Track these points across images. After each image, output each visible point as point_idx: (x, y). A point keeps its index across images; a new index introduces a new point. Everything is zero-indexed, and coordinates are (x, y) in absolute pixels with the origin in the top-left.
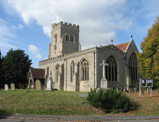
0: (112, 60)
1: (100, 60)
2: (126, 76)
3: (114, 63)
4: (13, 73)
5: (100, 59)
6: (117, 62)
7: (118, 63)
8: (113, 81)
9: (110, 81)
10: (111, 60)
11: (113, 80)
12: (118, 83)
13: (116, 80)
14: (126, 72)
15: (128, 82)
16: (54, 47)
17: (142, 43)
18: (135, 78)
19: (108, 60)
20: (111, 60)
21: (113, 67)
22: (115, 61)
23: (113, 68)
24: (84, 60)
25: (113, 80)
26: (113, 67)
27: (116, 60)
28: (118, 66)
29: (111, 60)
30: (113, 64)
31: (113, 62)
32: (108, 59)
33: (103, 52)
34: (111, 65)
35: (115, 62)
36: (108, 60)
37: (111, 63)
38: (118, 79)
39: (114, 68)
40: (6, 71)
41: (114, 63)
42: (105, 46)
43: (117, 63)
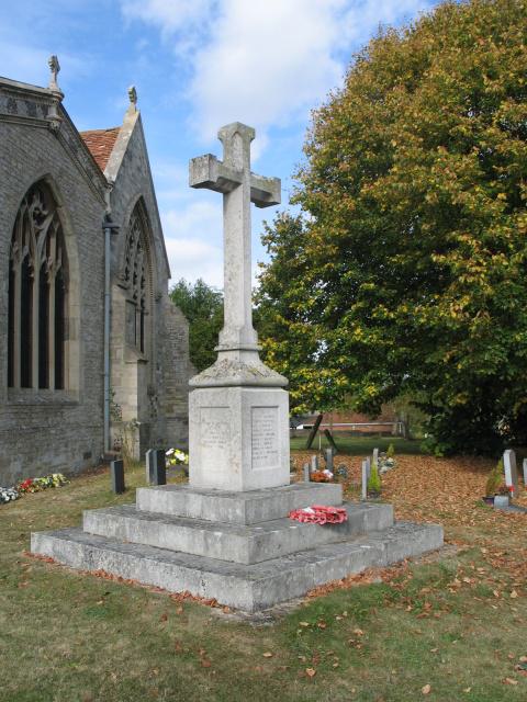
0: (45, 217)
2: (120, 352)
3: (53, 241)
6: (70, 242)
7: (80, 251)
9: (28, 390)
10: (40, 219)
11: (43, 384)
12: (74, 404)
13: (59, 385)
14: (115, 323)
15: (133, 400)
16: (192, 361)
18: (31, 280)
22: (60, 228)
24: (194, 161)
25: (43, 384)
27: (67, 228)
28: (75, 275)
32: (23, 202)
35: (61, 244)
37: (37, 235)
38: (73, 378)
41: (53, 241)
42: (13, 84)
43: (72, 253)
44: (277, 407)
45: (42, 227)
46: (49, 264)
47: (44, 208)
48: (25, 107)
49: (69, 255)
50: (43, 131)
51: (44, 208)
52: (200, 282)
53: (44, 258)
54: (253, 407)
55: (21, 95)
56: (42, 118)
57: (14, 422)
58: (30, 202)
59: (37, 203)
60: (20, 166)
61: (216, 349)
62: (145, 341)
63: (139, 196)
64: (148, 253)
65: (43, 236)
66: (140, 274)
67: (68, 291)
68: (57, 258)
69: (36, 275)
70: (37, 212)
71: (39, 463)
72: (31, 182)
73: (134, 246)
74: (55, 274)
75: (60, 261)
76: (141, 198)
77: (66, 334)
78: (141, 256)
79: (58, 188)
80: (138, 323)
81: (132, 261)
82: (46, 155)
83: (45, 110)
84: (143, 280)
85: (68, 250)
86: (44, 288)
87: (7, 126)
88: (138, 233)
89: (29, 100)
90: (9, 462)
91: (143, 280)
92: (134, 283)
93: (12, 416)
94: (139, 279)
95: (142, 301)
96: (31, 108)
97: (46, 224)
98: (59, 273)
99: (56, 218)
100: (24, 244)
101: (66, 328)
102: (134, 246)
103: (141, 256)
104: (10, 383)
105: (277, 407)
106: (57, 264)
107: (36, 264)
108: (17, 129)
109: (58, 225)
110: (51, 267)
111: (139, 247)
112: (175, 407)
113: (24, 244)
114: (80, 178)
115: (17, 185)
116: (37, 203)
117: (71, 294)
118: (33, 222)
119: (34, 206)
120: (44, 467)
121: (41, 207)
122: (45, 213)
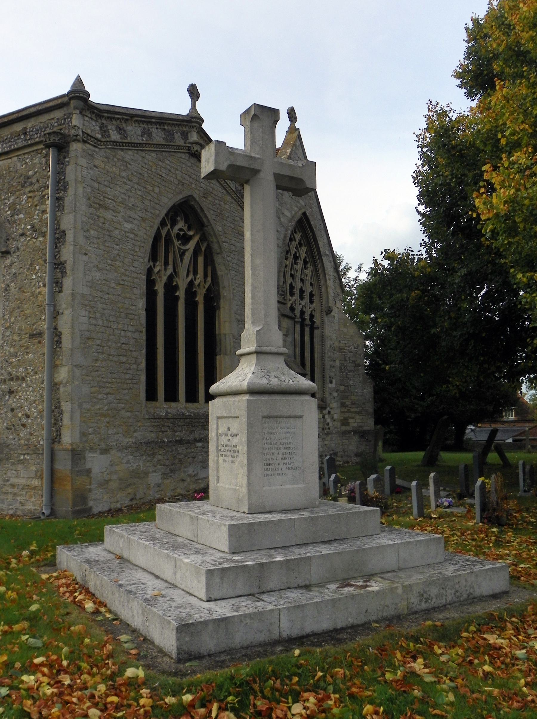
0: (190, 238)
1: (108, 215)
3: (201, 260)
4: (443, 658)
5: (107, 208)
8: (192, 406)
10: (186, 239)
17: (476, 21)
19: (164, 232)
20: (178, 237)
21: (191, 293)
22: (209, 249)
23: (196, 304)
26: (191, 293)
29: (178, 237)
30: (195, 273)
31: (198, 246)
32: (163, 223)
33: (129, 155)
34: (182, 270)
36: (164, 232)
37: (182, 254)
39: (200, 298)
40: (66, 683)
41: (201, 260)
44: (301, 417)
45: (187, 247)
46: (197, 282)
47: (189, 229)
48: (162, 134)
49: (219, 273)
50: (183, 156)
51: (189, 229)
52: (66, 261)
53: (191, 276)
54: (218, 418)
55: (156, 123)
56: (182, 143)
57: (153, 435)
58: (174, 223)
59: (181, 224)
60: (157, 190)
61: (239, 352)
62: (316, 356)
63: (301, 212)
64: (316, 269)
65: (188, 256)
66: (308, 289)
67: (219, 308)
68: (206, 276)
69: (181, 293)
70: (182, 233)
71: (182, 474)
72: (170, 204)
73: (301, 262)
74: (204, 291)
75: (209, 279)
76: (304, 214)
77: (218, 350)
78: (308, 272)
79: (202, 210)
80: (298, 337)
81: (298, 275)
82: (187, 178)
83: (185, 136)
84: (311, 295)
85: (218, 268)
86: (191, 306)
87: (140, 152)
88: (304, 249)
89: (166, 127)
90: (146, 474)
91: (311, 295)
92: (302, 298)
93: (151, 429)
94: (307, 295)
95: (312, 316)
96: (170, 135)
97: (191, 245)
98: (209, 290)
99: (204, 238)
100: (166, 263)
101: (218, 343)
102: (301, 262)
103: (308, 272)
104: (151, 395)
105: (264, 417)
106: (205, 282)
107: (182, 283)
108: (153, 154)
109: (205, 244)
110: (199, 285)
111: (305, 262)
112: (351, 421)
113: (166, 263)
114: (229, 198)
115: (155, 208)
116: (181, 224)
117: (222, 310)
118: (177, 243)
119: (177, 227)
120: (188, 480)
121: (185, 229)
122: (191, 233)
